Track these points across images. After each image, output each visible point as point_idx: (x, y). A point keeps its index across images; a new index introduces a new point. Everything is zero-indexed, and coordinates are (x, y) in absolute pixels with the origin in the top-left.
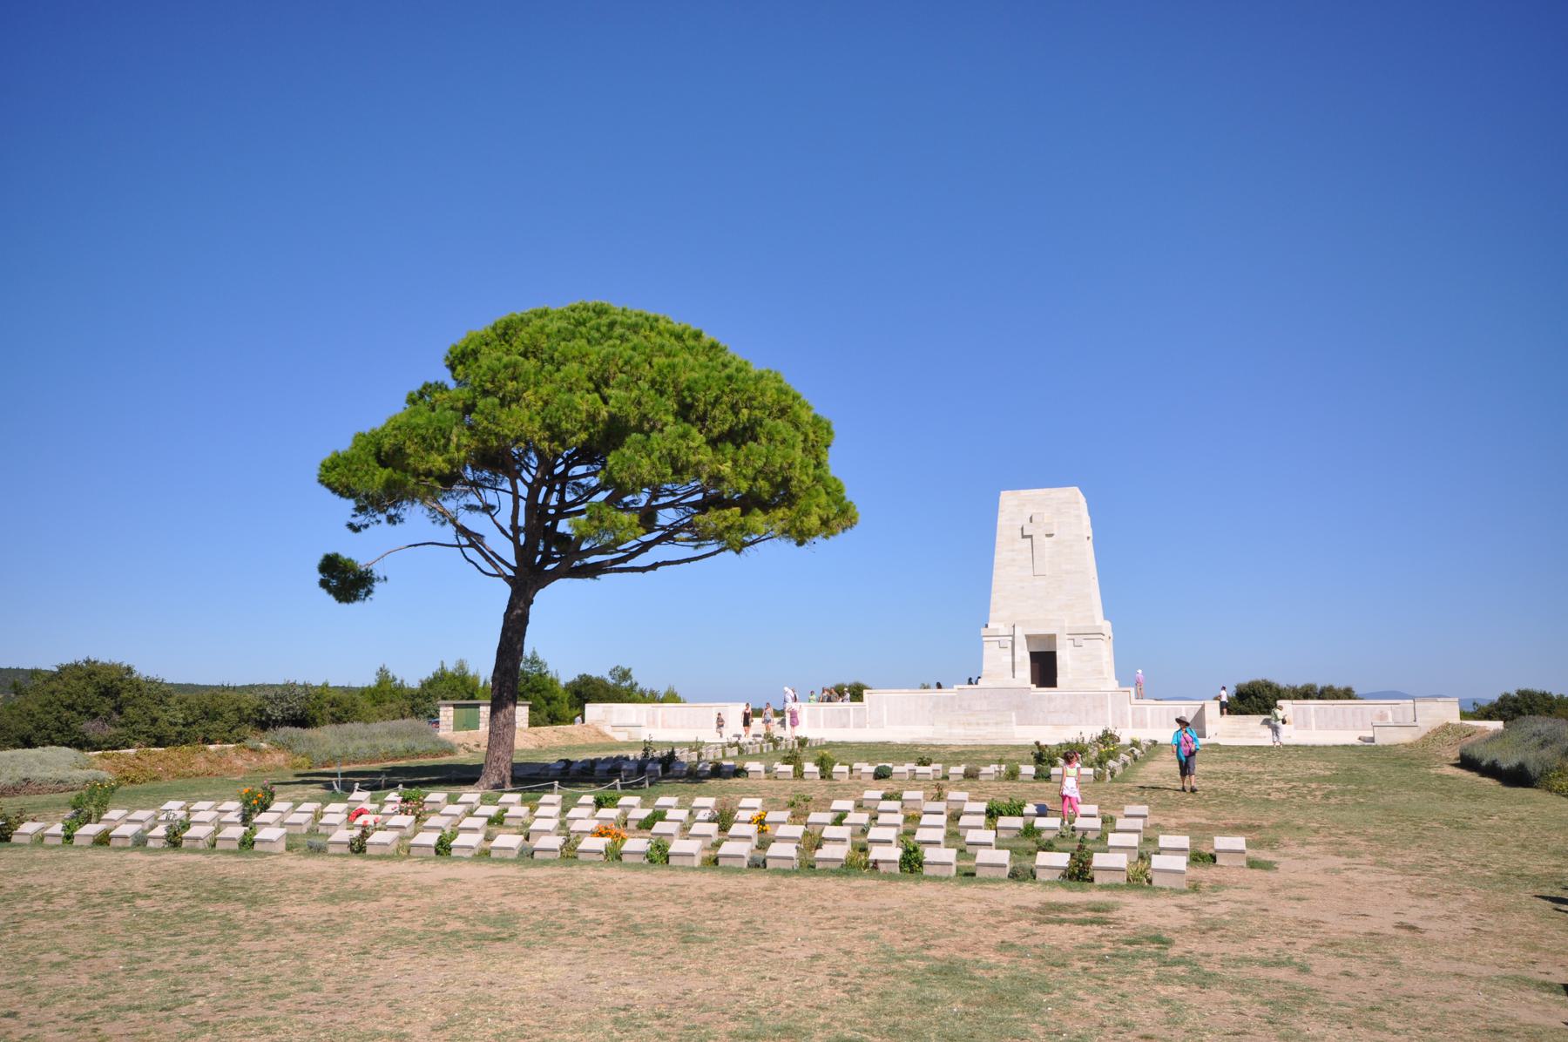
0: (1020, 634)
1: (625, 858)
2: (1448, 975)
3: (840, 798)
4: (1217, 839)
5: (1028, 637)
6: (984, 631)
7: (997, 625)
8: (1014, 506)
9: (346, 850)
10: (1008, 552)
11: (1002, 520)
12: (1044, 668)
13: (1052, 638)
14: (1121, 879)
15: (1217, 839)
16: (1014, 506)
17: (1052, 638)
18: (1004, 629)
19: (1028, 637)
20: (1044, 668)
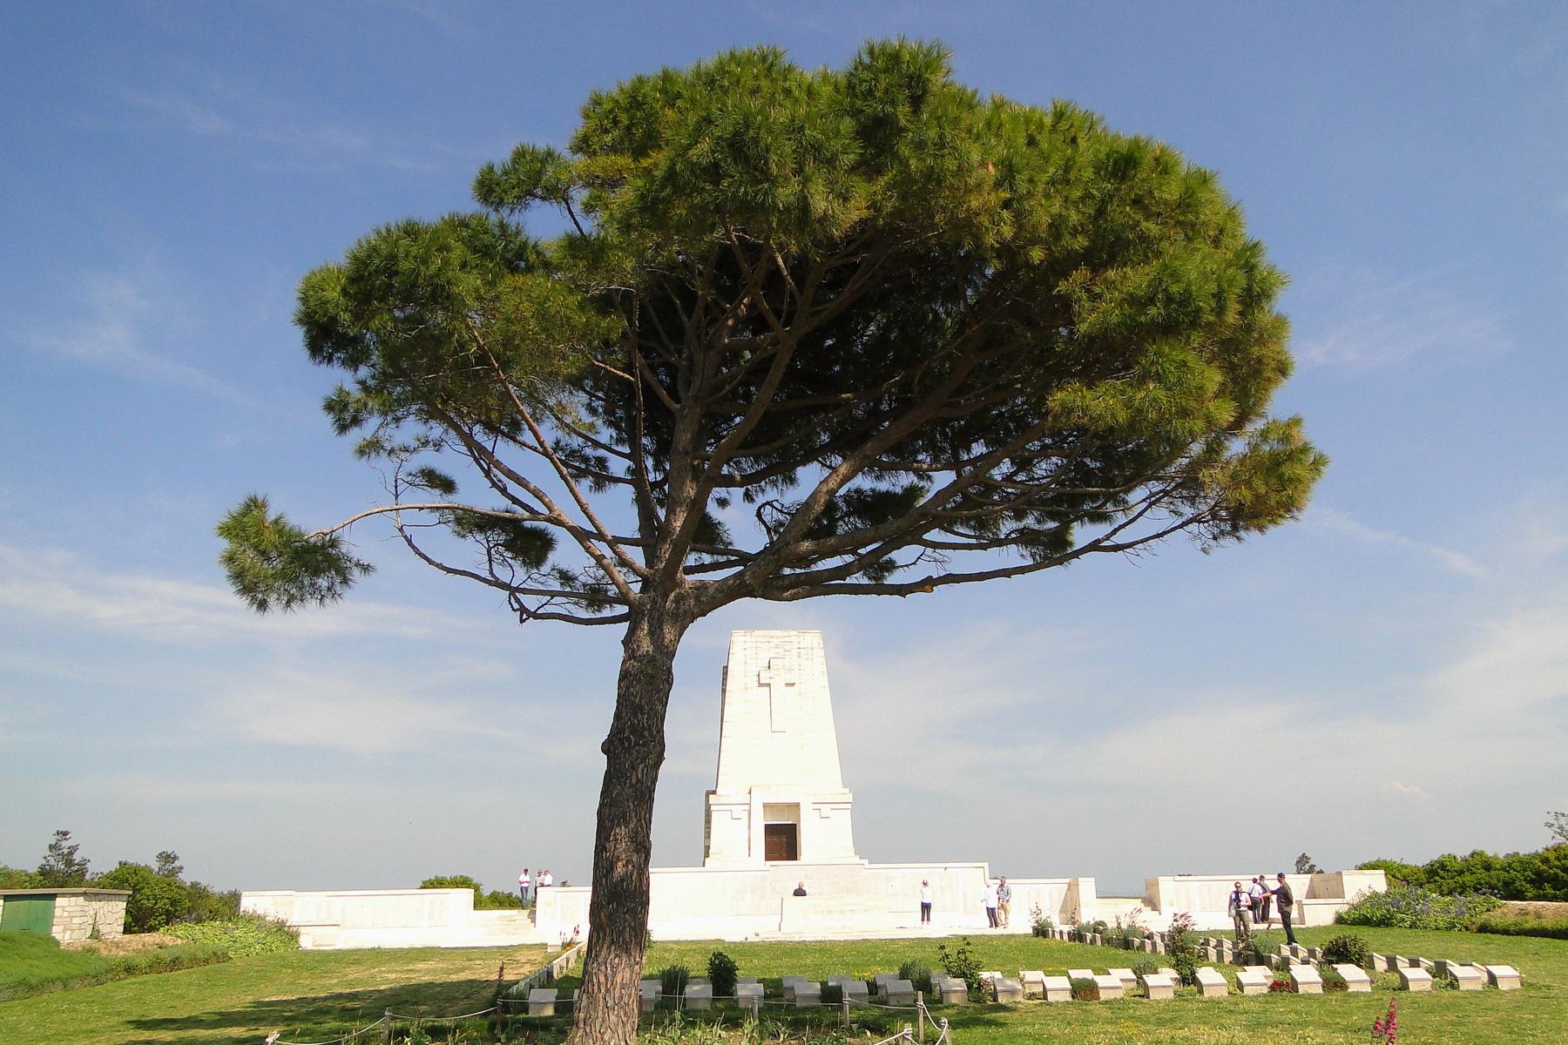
5: (765, 806)
7: (729, 789)
12: (783, 841)
20: (783, 841)
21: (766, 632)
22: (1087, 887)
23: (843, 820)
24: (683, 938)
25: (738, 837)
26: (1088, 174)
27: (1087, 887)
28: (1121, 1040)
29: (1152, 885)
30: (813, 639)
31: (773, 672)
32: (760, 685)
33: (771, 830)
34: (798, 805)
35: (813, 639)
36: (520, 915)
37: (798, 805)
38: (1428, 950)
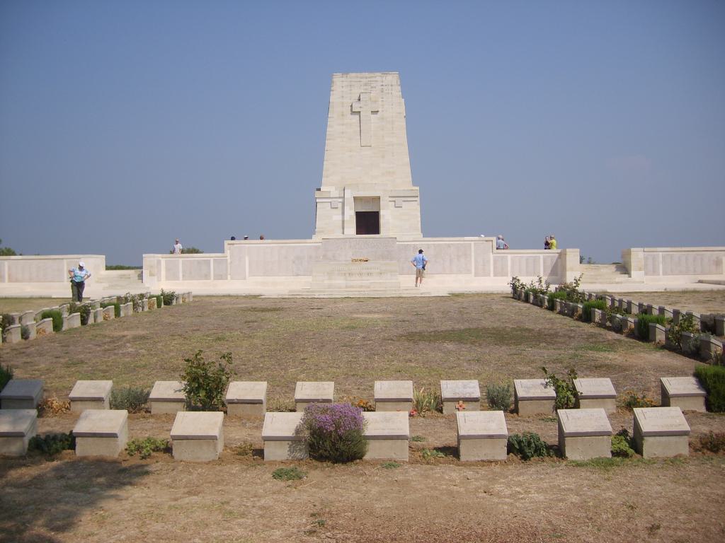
0: (349, 195)
1: (649, 446)
2: (371, 269)
3: (91, 376)
4: (378, 384)
5: (355, 198)
6: (317, 194)
7: (329, 187)
8: (344, 89)
9: (501, 453)
10: (339, 127)
11: (334, 98)
12: (368, 222)
13: (377, 200)
14: (604, 449)
15: (378, 384)
16: (344, 89)
17: (377, 200)
18: (335, 192)
19: (355, 198)
20: (368, 222)
21: (359, 74)
22: (573, 256)
23: (413, 210)
24: (232, 293)
25: (336, 221)
26: (698, 326)
27: (573, 256)
28: (464, 539)
29: (627, 254)
30: (392, 79)
31: (362, 104)
32: (353, 113)
33: (359, 215)
34: (379, 198)
35: (392, 79)
36: (132, 273)
37: (379, 198)
38: (659, 297)
